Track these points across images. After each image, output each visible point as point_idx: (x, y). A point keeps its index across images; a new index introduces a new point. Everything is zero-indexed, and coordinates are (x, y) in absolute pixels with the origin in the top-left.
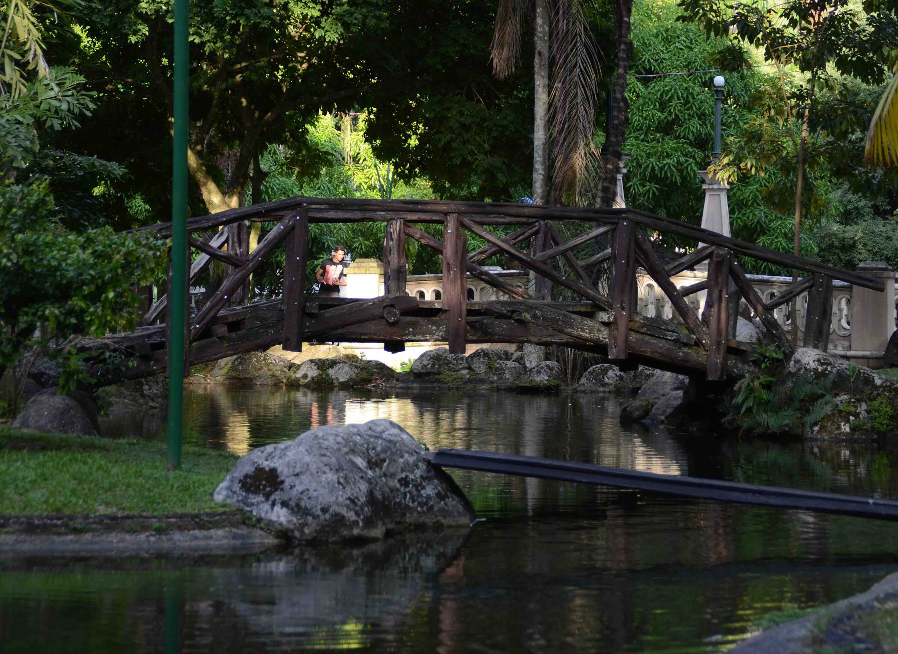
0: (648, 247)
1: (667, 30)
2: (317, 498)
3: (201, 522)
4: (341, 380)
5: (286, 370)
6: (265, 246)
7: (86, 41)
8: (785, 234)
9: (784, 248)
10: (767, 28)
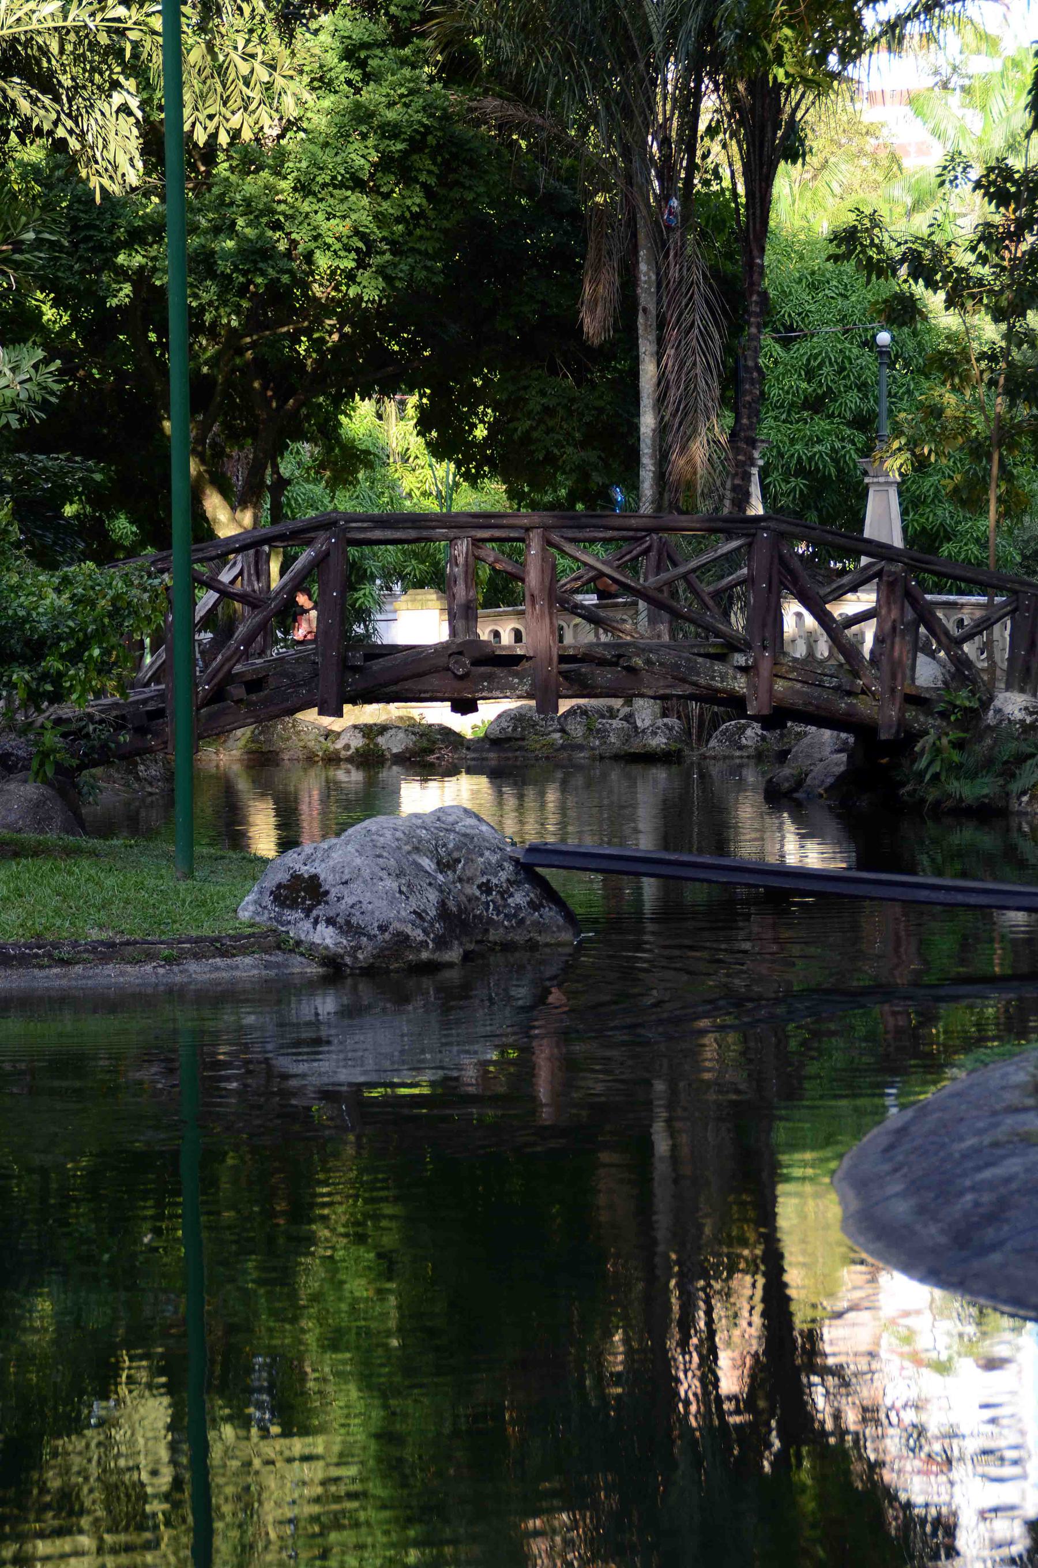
0: (796, 564)
1: (813, 273)
2: (373, 913)
3: (221, 947)
4: (395, 751)
5: (322, 739)
6: (291, 579)
7: (49, 313)
8: (977, 540)
9: (976, 557)
10: (947, 266)
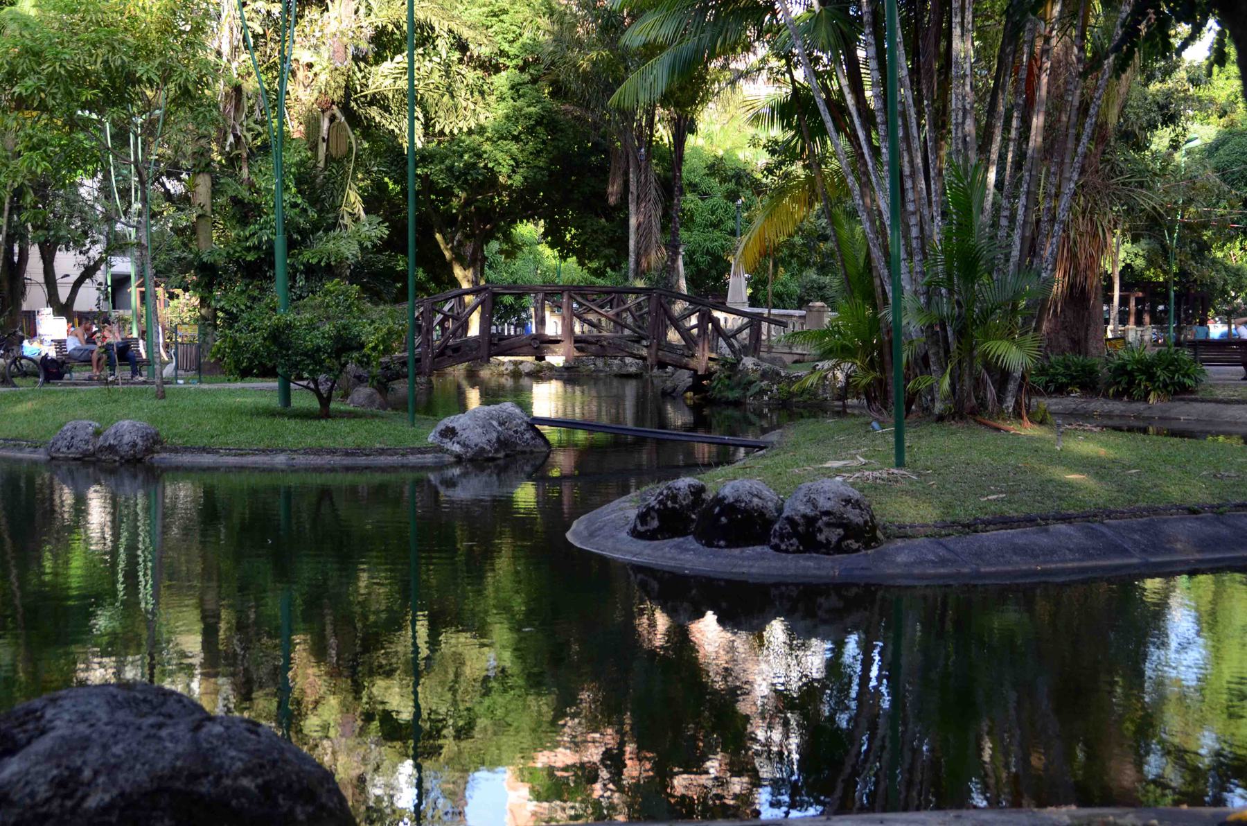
3: (421, 451)
7: (391, 186)
